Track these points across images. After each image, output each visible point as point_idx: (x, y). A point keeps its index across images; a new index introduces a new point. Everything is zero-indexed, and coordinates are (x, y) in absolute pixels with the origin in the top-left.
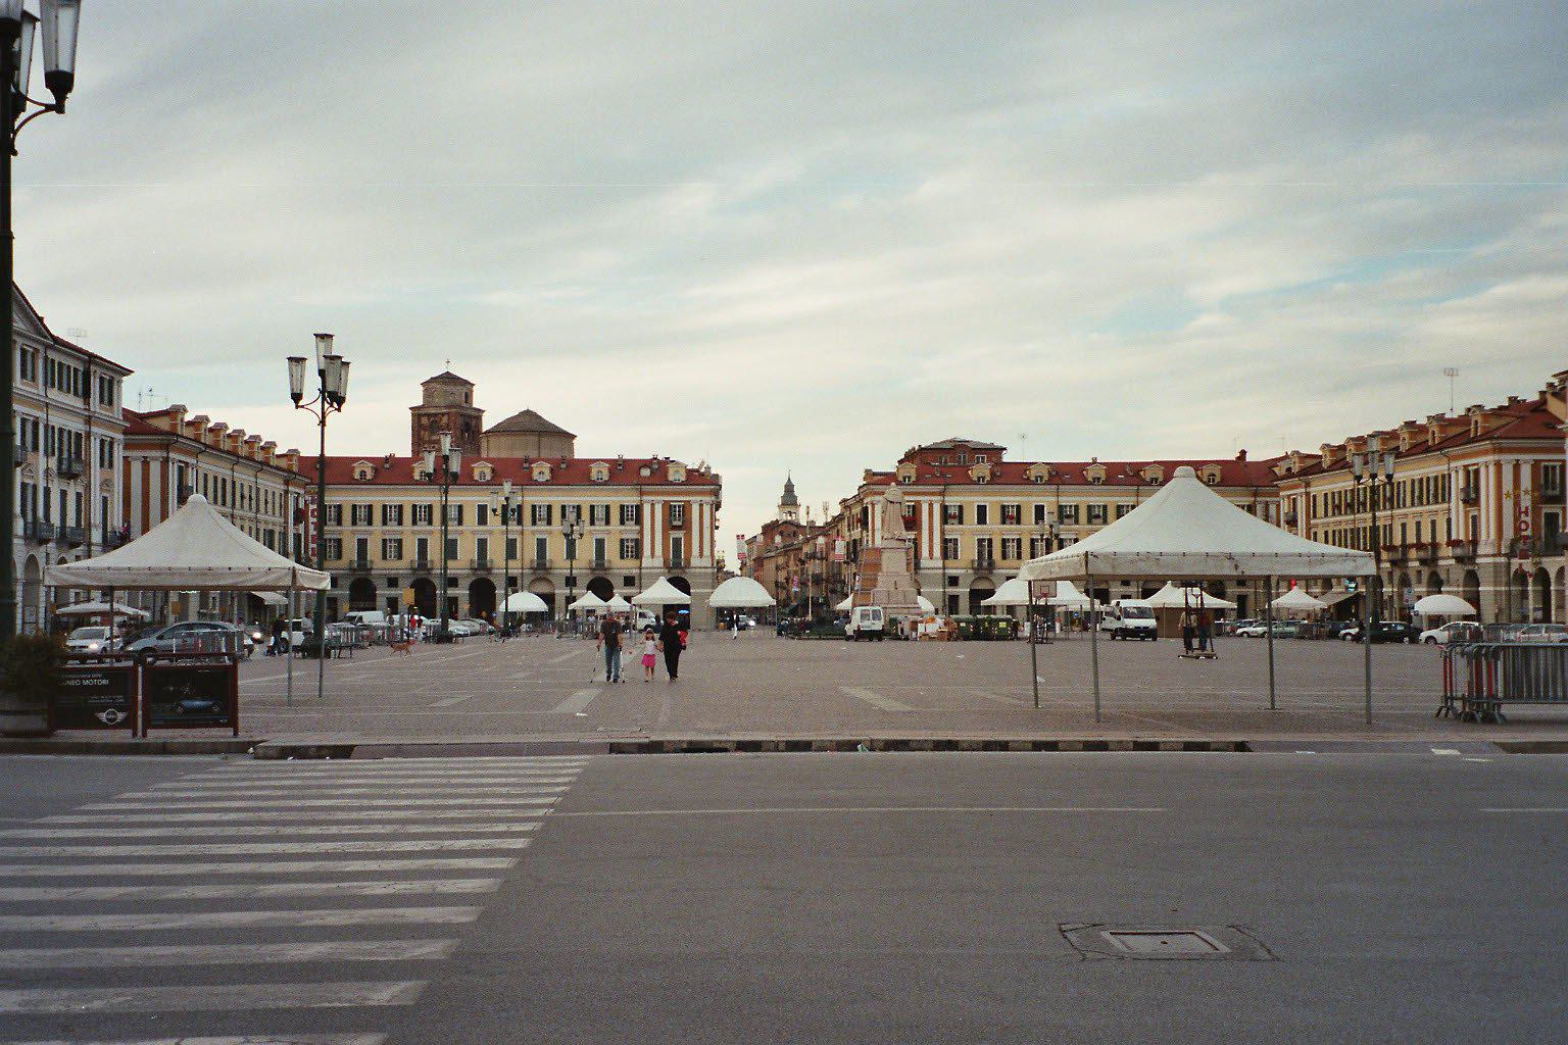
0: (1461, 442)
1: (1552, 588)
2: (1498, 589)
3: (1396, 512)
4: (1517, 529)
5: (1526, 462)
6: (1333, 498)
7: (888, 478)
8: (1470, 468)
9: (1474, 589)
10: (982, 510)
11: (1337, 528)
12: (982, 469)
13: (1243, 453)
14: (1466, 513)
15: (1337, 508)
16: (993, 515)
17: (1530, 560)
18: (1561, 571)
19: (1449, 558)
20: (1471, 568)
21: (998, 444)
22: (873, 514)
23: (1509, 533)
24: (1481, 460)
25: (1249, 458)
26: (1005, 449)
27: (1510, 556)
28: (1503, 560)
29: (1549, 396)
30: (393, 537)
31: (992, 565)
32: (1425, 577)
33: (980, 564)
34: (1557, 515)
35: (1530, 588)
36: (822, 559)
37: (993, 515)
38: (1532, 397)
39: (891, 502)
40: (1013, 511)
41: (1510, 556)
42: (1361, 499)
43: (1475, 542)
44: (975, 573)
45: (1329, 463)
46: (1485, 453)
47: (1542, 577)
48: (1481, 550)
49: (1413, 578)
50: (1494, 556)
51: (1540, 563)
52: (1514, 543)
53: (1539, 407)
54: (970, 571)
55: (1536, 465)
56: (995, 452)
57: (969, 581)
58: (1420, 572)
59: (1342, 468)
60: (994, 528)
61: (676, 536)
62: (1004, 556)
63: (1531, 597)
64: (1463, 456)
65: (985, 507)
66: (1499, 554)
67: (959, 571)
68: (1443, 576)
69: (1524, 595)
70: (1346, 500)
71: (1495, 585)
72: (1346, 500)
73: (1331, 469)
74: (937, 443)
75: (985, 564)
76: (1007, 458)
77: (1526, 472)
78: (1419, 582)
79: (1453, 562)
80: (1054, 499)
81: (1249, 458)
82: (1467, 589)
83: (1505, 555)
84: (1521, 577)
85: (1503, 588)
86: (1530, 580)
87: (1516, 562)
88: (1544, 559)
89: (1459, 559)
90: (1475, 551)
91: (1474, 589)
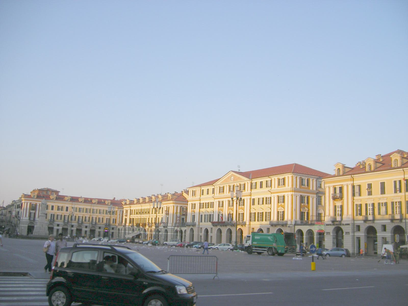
0: (166, 200)
1: (183, 234)
2: (172, 234)
3: (142, 215)
4: (176, 220)
5: (29, 202)
6: (139, 210)
7: (29, 196)
8: (167, 207)
9: (145, 233)
10: (53, 207)
11: (137, 218)
12: (53, 196)
13: (115, 198)
14: (166, 217)
15: (137, 213)
16: (55, 208)
17: (179, 228)
18: (185, 230)
19: (162, 226)
20: (166, 229)
21: (58, 190)
22: (24, 205)
23: (175, 222)
24: (170, 205)
25: (116, 199)
26: (60, 192)
27: (174, 227)
28: (173, 227)
29: (183, 192)
30: (397, 215)
31: (54, 221)
32: (137, 229)
33: (51, 220)
34: (184, 218)
35: (178, 234)
36: (4, 216)
37: (55, 208)
38: (179, 192)
39: (43, 204)
40: (34, 205)
41: (174, 227)
42: (143, 211)
43: (167, 223)
44: (49, 223)
45: (136, 203)
46: (171, 203)
47: (181, 232)
48: (169, 225)
49: (147, 230)
50: (171, 226)
51: (181, 229)
52: (176, 223)
53: (181, 195)
54: (48, 222)
55: (30, 203)
56: (57, 192)
57: (90, 227)
58: (142, 229)
59: (139, 204)
60: (55, 211)
61: (183, 217)
62: (57, 219)
63: (178, 236)
64: (166, 204)
65: (53, 206)
66: (172, 226)
67: (60, 223)
68: (160, 230)
69: (177, 235)
70: (148, 211)
71: (171, 233)
72: (148, 211)
73: (136, 204)
74: (42, 189)
75: (52, 220)
76: (60, 194)
77: (29, 204)
78: (130, 230)
79: (163, 227)
80: (71, 205)
81: (116, 199)
82: (165, 233)
83: (174, 226)
84: (177, 231)
85: (173, 234)
86: (179, 232)
87: (176, 228)
88: (182, 228)
89: (164, 227)
90: (167, 225)
91: (145, 233)
